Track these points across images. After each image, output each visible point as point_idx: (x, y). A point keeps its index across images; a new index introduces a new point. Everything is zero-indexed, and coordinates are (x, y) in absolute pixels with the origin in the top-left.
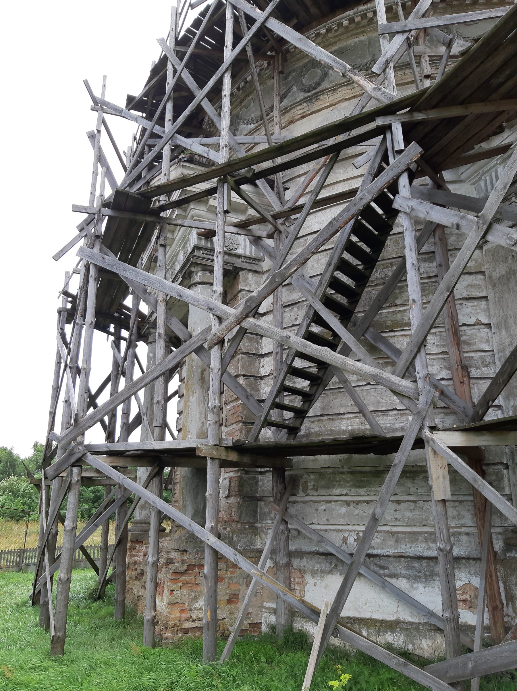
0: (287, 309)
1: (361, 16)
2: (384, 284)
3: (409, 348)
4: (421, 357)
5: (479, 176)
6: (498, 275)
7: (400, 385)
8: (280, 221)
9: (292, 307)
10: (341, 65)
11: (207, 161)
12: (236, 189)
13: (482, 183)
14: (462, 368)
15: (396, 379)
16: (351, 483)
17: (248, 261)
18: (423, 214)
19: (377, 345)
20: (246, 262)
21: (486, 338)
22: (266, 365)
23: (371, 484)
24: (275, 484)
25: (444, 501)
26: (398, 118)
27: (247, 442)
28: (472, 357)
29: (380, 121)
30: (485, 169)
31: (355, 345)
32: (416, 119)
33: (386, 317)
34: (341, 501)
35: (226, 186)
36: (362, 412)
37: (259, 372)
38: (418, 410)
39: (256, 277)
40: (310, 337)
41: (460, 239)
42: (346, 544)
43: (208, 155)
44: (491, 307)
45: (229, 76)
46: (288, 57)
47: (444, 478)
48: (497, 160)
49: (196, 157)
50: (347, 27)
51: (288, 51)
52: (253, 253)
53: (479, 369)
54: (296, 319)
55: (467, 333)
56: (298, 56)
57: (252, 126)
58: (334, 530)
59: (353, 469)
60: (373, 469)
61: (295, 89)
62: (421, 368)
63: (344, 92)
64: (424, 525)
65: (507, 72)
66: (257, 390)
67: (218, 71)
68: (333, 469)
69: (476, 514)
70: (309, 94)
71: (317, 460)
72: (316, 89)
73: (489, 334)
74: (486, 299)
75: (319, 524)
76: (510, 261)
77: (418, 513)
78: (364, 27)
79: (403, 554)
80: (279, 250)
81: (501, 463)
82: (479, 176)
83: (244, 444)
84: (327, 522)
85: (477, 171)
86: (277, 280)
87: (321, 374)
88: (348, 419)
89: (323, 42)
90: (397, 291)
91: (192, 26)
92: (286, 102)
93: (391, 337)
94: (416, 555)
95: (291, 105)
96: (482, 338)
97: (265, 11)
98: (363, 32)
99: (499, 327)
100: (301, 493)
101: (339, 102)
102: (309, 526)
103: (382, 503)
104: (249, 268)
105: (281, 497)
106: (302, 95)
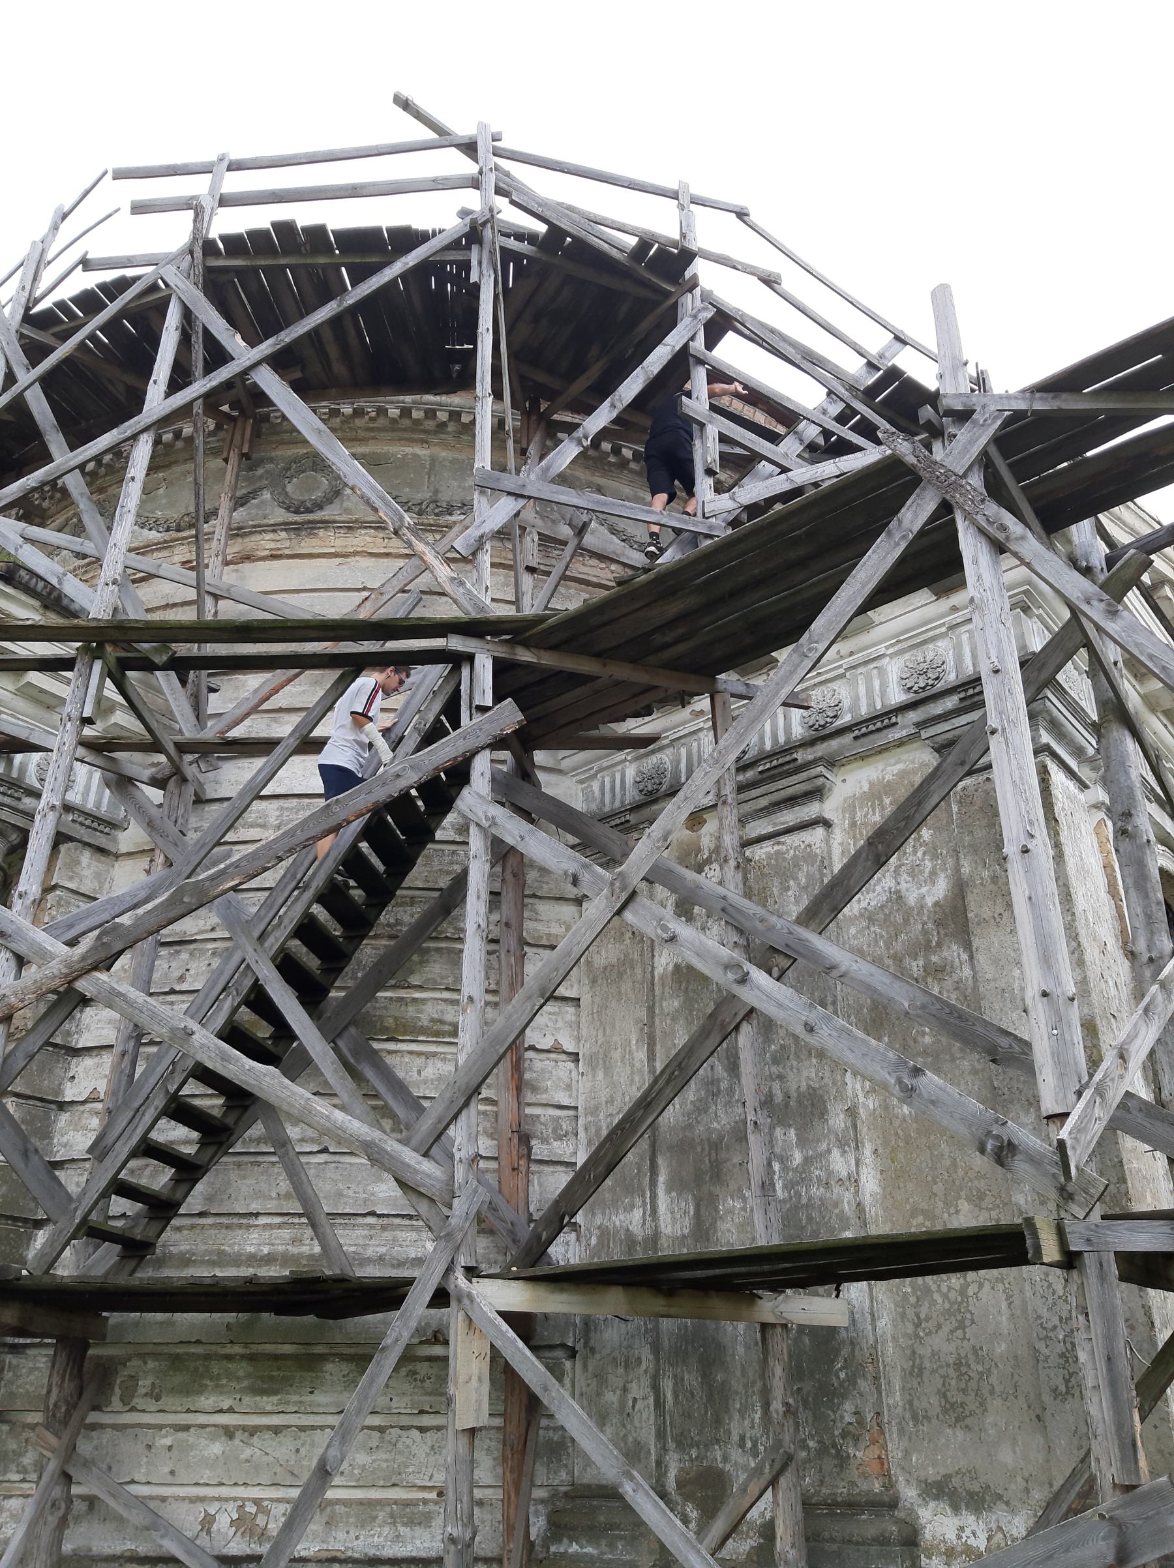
0: (164, 952)
1: (426, 411)
2: (391, 937)
3: (448, 1095)
4: (469, 1117)
5: (592, 772)
6: (603, 962)
7: (416, 1171)
8: (189, 758)
9: (178, 948)
10: (395, 511)
11: (45, 587)
12: (118, 676)
13: (596, 786)
14: (520, 1139)
15: (409, 1156)
16: (245, 1383)
17: (88, 822)
18: (514, 837)
19: (360, 1068)
20: (82, 824)
21: (567, 1080)
22: (81, 1075)
23: (291, 1386)
24: (56, 1379)
25: (472, 1431)
26: (489, 647)
27: (24, 1272)
28: (538, 1116)
29: (455, 643)
30: (605, 763)
31: (335, 1071)
32: (518, 658)
33: (386, 1008)
34: (215, 1426)
35: (98, 666)
36: (310, 1215)
37: (59, 1091)
38: (449, 1229)
39: (99, 862)
40: (233, 1035)
41: (546, 879)
42: (209, 1532)
43: (60, 583)
44: (583, 1020)
45: (150, 443)
46: (264, 430)
47: (480, 1379)
48: (628, 754)
49: (23, 573)
50: (394, 421)
51: (266, 418)
52: (104, 808)
53: (548, 1143)
54: (182, 979)
55: (537, 1065)
56: (286, 436)
57: (154, 536)
58: (184, 1499)
59: (254, 1349)
60: (302, 1350)
61: (266, 495)
62: (465, 1142)
63: (368, 539)
64: (394, 1485)
65: (681, 631)
66: (47, 1135)
67: (127, 424)
68: (208, 1347)
69: (505, 1459)
70: (297, 518)
71: (172, 1323)
72: (312, 512)
73: (574, 1074)
74: (575, 1003)
75: (149, 1483)
76: (628, 942)
77: (384, 1456)
78: (425, 432)
79: (339, 1554)
80: (173, 818)
81: (563, 1346)
82: (592, 772)
83: (18, 1279)
84: (170, 1477)
85: (591, 762)
86: (186, 899)
87: (230, 1121)
88: (270, 1226)
89: (341, 429)
90: (415, 958)
91: (76, 300)
92: (240, 515)
93: (390, 1052)
94: (366, 1555)
95: (254, 526)
96: (559, 1079)
97: (256, 349)
98: (423, 441)
99: (592, 1065)
100: (116, 1403)
101: (355, 554)
102: (127, 1487)
103: (344, 1435)
104: (86, 839)
105: (68, 1415)
106: (280, 515)
